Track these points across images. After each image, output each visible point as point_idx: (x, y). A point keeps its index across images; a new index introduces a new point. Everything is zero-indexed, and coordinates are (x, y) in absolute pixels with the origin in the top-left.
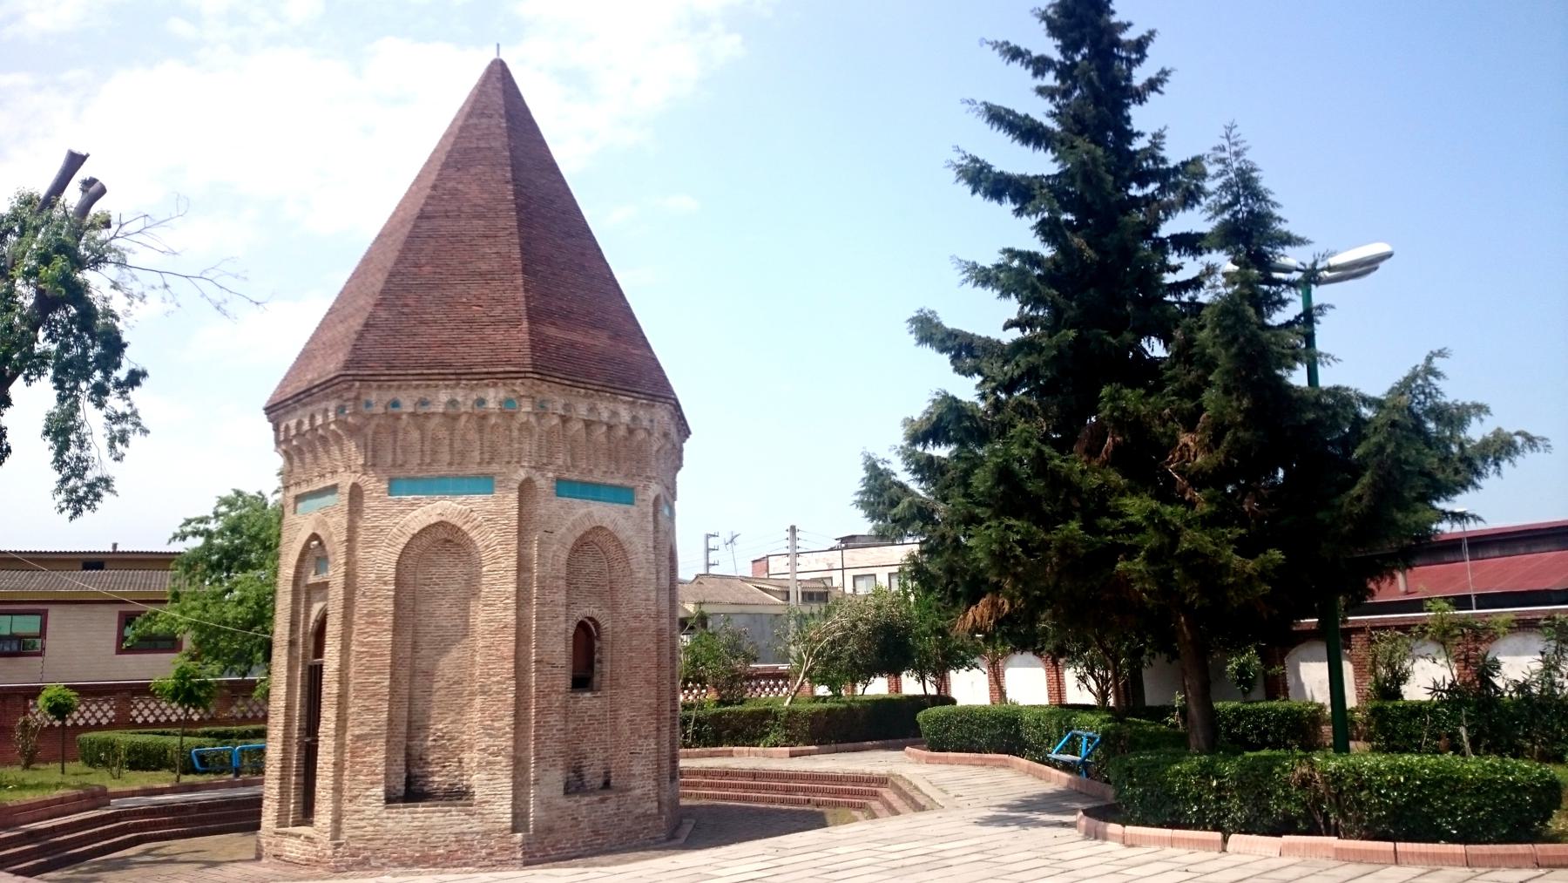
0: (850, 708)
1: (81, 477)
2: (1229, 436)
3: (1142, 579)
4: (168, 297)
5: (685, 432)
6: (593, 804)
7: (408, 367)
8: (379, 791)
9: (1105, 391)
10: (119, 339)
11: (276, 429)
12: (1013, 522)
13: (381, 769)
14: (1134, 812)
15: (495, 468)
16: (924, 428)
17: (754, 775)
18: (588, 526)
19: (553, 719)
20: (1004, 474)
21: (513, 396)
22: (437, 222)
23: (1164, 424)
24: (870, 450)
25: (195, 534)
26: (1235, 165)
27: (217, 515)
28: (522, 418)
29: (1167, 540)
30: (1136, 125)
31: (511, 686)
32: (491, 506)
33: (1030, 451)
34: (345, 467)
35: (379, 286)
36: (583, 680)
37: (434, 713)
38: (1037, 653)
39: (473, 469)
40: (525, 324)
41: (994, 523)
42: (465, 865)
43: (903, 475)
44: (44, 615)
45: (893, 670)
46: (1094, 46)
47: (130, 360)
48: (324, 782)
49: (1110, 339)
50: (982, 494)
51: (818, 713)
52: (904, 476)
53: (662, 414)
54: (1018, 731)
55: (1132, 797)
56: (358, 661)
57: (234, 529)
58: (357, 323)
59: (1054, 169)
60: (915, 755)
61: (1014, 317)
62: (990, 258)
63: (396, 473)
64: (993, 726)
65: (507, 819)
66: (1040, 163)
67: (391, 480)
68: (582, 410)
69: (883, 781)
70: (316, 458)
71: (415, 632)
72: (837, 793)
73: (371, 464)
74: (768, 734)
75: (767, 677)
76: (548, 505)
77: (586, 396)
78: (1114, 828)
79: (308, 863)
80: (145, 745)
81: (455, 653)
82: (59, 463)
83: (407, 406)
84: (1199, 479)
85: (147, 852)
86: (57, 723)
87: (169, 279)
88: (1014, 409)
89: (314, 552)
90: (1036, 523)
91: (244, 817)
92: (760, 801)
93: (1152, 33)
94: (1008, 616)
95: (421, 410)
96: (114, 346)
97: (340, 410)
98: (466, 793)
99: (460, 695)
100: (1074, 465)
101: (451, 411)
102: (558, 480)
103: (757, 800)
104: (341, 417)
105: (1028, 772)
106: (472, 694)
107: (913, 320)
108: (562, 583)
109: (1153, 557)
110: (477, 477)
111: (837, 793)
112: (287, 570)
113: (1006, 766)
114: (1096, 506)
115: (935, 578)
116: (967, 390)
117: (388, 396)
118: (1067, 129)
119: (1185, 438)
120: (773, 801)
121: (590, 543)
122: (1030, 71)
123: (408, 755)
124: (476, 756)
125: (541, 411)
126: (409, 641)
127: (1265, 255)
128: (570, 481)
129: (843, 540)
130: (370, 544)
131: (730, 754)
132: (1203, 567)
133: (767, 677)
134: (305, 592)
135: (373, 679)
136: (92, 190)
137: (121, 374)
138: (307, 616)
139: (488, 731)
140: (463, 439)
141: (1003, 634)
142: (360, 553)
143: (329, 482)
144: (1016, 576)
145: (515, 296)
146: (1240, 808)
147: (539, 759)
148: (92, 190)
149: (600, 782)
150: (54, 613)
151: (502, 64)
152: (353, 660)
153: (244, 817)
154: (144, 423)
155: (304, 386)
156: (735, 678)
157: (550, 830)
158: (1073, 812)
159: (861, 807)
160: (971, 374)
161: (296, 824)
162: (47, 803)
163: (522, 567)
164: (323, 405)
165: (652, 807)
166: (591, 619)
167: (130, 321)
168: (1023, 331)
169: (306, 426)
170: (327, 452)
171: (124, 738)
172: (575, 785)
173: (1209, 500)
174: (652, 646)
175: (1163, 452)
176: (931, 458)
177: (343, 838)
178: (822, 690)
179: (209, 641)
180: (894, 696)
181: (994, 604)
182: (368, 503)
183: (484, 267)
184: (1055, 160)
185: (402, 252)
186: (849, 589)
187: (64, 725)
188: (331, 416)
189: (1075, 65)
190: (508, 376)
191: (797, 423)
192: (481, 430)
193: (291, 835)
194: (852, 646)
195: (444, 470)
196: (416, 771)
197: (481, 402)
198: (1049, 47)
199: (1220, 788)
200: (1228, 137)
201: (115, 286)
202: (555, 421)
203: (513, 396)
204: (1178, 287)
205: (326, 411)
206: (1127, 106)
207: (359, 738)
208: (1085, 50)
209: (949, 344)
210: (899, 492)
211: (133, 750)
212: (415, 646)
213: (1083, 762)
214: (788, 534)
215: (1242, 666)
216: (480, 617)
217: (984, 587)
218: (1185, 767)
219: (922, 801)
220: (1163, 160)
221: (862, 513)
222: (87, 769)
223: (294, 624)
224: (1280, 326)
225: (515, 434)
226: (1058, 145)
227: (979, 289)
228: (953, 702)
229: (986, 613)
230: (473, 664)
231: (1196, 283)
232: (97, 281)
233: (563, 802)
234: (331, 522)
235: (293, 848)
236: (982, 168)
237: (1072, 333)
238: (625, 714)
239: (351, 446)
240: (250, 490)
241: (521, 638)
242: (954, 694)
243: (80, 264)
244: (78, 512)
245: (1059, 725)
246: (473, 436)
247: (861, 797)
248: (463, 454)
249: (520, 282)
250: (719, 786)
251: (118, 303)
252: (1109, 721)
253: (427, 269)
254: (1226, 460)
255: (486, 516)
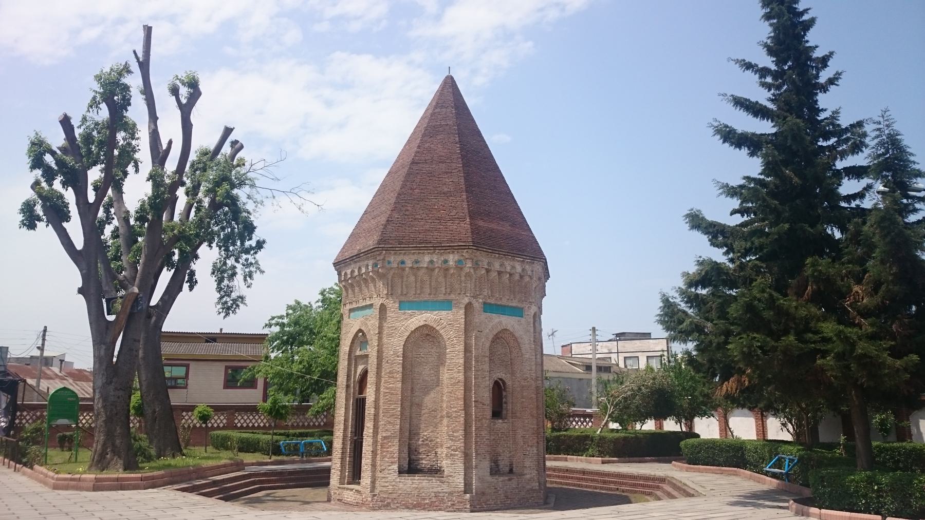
0: (636, 437)
1: (229, 296)
2: (883, 288)
3: (832, 369)
4: (275, 203)
5: (547, 276)
6: (501, 480)
7: (409, 243)
8: (395, 467)
9: (809, 260)
10: (252, 224)
11: (339, 274)
12: (755, 335)
13: (396, 455)
14: (824, 502)
15: (452, 296)
16: (697, 278)
17: (584, 472)
18: (499, 329)
19: (484, 433)
20: (749, 307)
21: (462, 258)
22: (421, 166)
23: (842, 280)
24: (665, 291)
25: (277, 324)
26: (887, 132)
27: (288, 314)
28: (467, 270)
29: (848, 348)
30: (821, 105)
31: (462, 414)
32: (451, 317)
33: (766, 295)
34: (377, 295)
35: (393, 200)
36: (497, 413)
37: (422, 426)
38: (750, 409)
39: (441, 297)
40: (468, 220)
41: (744, 336)
42: (440, 510)
43: (678, 300)
44: (187, 366)
45: (660, 416)
46: (796, 60)
47: (257, 235)
48: (366, 461)
49: (809, 229)
50: (735, 318)
51: (617, 439)
52: (683, 306)
53: (538, 267)
54: (743, 454)
55: (824, 493)
56: (382, 396)
57: (296, 323)
58: (383, 219)
59: (774, 130)
60: (679, 466)
61: (737, 207)
62: (736, 181)
63: (403, 298)
64: (728, 451)
65: (462, 486)
66: (766, 127)
67: (400, 302)
68: (497, 266)
69: (663, 480)
70: (361, 290)
71: (413, 383)
72: (635, 485)
73: (390, 294)
74: (588, 449)
75: (579, 416)
76: (480, 317)
77: (498, 258)
78: (814, 510)
79: (357, 505)
80: (247, 439)
81: (432, 395)
82: (219, 289)
83: (409, 264)
84: (865, 313)
85: (268, 495)
86: (204, 425)
87: (275, 193)
88: (752, 269)
89: (360, 338)
90: (768, 335)
91: (320, 479)
92: (588, 487)
93: (831, 53)
94: (747, 388)
95: (415, 266)
96: (249, 228)
97: (375, 265)
98: (439, 470)
99: (435, 417)
100: (790, 303)
101: (430, 266)
102: (485, 303)
103: (586, 486)
104: (376, 269)
105: (750, 478)
106: (442, 417)
107: (687, 216)
108: (487, 359)
109: (840, 357)
110: (443, 301)
111: (635, 485)
112: (345, 348)
113: (736, 475)
114: (804, 328)
115: (701, 365)
116: (719, 256)
117: (400, 258)
118: (779, 108)
119: (856, 288)
120: (596, 488)
121: (501, 338)
122: (757, 76)
123: (409, 448)
124: (445, 451)
125: (476, 266)
126: (410, 388)
127: (905, 183)
128: (490, 304)
129: (617, 335)
130: (390, 335)
131: (566, 460)
132: (869, 363)
133: (579, 416)
134: (353, 360)
135: (392, 407)
136: (237, 146)
137: (253, 243)
138: (356, 372)
139: (451, 438)
140: (436, 281)
141: (744, 398)
142: (385, 340)
143: (368, 303)
144: (757, 367)
145: (461, 203)
146: (892, 503)
147: (477, 454)
148: (237, 146)
149: (507, 469)
150: (193, 365)
151: (452, 78)
152: (381, 396)
153: (320, 479)
154: (262, 268)
155: (356, 252)
156: (562, 416)
157: (483, 494)
158: (787, 501)
159: (650, 494)
160: (722, 247)
161: (349, 483)
162: (219, 467)
163: (467, 350)
164: (366, 263)
165: (536, 485)
166: (501, 379)
167: (257, 215)
168: (743, 216)
169: (356, 273)
170: (367, 287)
171: (235, 434)
172: (495, 470)
173: (872, 325)
174: (534, 396)
175: (843, 296)
176: (697, 295)
177: (377, 492)
178: (614, 426)
179: (284, 382)
180: (659, 431)
181: (739, 381)
182: (389, 314)
183: (446, 190)
184: (774, 126)
185: (404, 182)
186: (622, 365)
187: (207, 426)
188: (370, 268)
189: (784, 70)
190: (460, 248)
191: (616, 272)
192: (445, 277)
193: (348, 489)
194: (637, 400)
195: (426, 297)
196: (413, 457)
197: (446, 261)
198: (768, 62)
199: (879, 490)
200: (883, 116)
201: (249, 197)
202: (483, 272)
203: (462, 258)
204: (849, 198)
205: (368, 266)
206: (817, 94)
207: (385, 438)
208: (790, 63)
209: (711, 230)
210: (683, 316)
211: (241, 441)
212: (412, 389)
213: (787, 474)
214: (591, 332)
215: (882, 420)
216: (445, 376)
217: (733, 372)
218: (857, 478)
219: (692, 492)
220: (839, 125)
221: (660, 327)
222: (215, 451)
223: (348, 376)
224: (913, 223)
225: (463, 278)
226: (776, 119)
227: (728, 198)
228: (698, 436)
229: (734, 386)
230: (442, 401)
231: (860, 195)
232: (241, 193)
233: (489, 479)
234: (369, 323)
235: (349, 496)
236: (730, 131)
237: (787, 226)
238: (520, 432)
239: (380, 284)
240: (304, 302)
241: (467, 389)
242: (697, 430)
243: (233, 186)
244: (227, 314)
245: (770, 452)
246: (441, 279)
247: (650, 488)
248: (436, 289)
249: (464, 197)
250: (563, 477)
251: (250, 206)
252: (803, 450)
253: (417, 191)
254: (882, 302)
255: (447, 321)
